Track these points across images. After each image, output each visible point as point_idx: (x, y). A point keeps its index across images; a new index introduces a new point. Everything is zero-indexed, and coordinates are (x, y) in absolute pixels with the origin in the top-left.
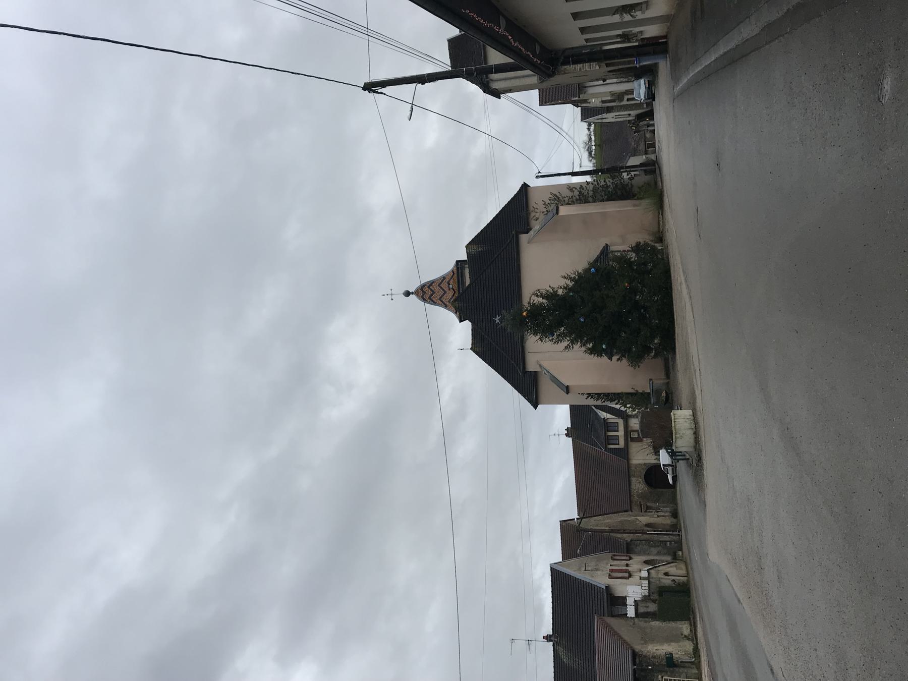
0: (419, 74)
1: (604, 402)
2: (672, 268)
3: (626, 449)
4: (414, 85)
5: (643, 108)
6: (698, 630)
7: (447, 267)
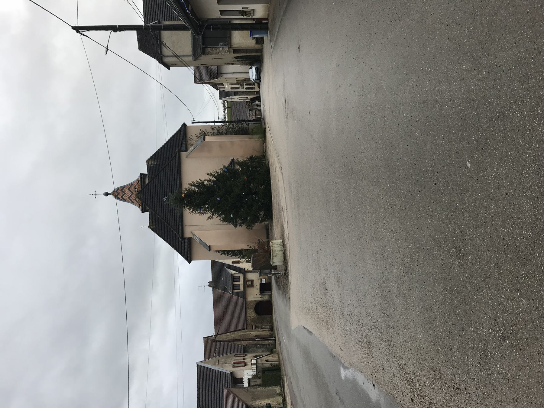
0: (113, 25)
2: (271, 167)
4: (110, 31)
5: (255, 95)
6: (285, 387)
7: (135, 177)
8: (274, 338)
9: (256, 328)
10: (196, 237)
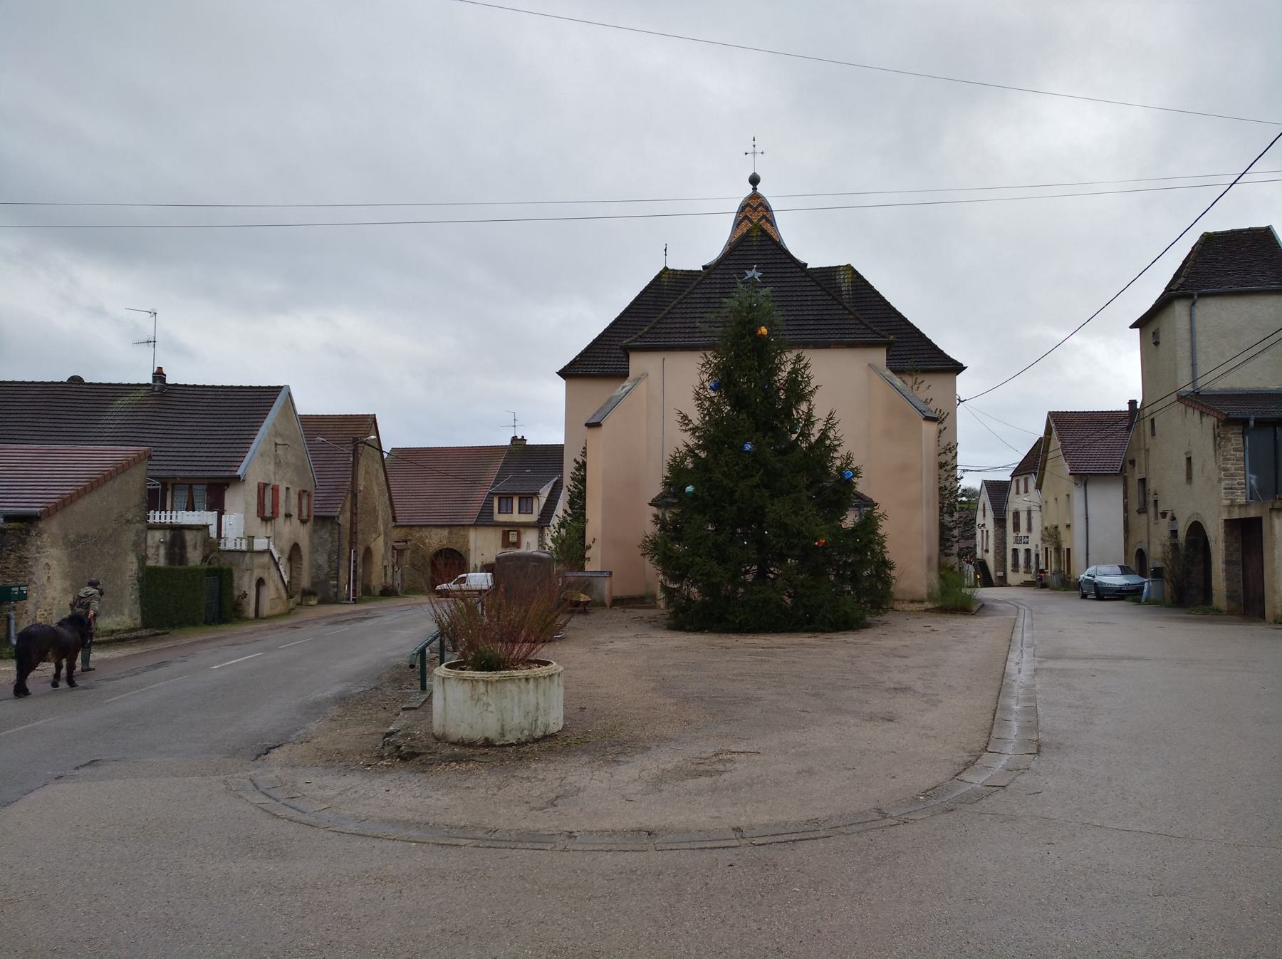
1: (569, 490)
3: (491, 523)
5: (996, 571)
8: (353, 600)
9: (397, 550)
10: (630, 387)
